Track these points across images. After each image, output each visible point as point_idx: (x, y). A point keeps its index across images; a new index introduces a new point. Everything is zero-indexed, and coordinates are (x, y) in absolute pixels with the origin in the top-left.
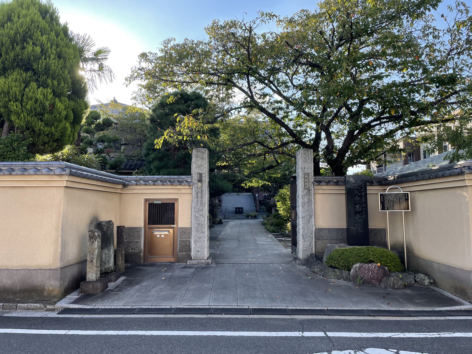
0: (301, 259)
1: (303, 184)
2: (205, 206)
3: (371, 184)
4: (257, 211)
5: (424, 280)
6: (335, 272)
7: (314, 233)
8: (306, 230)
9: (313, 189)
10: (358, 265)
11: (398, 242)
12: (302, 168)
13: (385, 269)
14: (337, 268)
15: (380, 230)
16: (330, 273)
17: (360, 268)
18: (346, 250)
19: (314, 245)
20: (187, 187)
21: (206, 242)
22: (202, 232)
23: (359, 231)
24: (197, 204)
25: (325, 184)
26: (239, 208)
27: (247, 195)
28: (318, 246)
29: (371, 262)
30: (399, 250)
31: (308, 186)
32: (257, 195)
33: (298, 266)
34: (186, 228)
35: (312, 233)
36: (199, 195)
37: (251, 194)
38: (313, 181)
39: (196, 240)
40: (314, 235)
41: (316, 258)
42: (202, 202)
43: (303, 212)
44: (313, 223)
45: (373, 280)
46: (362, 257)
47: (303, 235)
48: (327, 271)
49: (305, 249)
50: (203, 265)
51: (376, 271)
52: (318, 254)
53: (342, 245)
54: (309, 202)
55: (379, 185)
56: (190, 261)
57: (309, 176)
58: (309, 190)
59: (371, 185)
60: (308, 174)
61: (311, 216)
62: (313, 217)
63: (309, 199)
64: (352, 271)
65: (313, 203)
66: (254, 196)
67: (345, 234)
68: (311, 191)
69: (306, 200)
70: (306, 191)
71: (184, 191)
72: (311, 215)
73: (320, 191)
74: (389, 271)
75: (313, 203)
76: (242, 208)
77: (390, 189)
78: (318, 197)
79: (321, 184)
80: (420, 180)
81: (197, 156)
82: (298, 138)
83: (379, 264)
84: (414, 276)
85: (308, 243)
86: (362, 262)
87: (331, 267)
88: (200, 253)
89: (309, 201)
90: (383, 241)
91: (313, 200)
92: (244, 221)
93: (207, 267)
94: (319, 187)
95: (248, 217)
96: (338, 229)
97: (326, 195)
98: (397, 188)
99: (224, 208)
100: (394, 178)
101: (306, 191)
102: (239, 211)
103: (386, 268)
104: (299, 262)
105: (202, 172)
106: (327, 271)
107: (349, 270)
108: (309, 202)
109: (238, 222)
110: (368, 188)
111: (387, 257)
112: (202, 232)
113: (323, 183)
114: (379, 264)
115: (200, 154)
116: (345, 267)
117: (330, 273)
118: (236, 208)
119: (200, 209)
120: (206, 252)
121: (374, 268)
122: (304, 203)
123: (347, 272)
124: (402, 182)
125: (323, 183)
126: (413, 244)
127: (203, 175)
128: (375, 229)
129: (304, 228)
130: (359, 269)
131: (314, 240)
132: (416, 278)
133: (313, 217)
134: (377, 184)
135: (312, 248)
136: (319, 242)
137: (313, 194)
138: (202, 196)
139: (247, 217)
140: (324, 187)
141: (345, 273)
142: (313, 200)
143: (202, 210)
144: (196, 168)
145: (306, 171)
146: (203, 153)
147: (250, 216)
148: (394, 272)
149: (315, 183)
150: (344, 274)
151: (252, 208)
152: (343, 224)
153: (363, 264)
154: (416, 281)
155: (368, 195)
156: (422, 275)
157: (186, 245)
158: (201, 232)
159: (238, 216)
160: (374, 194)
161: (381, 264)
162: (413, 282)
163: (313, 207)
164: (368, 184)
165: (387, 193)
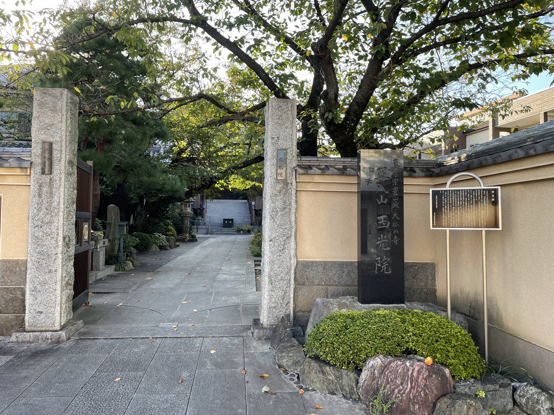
0: (265, 325)
1: (274, 171)
2: (57, 214)
3: (411, 172)
4: (252, 224)
5: (538, 402)
6: (323, 373)
7: (292, 272)
8: (276, 267)
9: (294, 183)
10: (377, 361)
11: (462, 292)
12: (273, 138)
13: (444, 375)
14: (328, 364)
15: (423, 266)
16: (313, 375)
17: (384, 368)
18: (353, 318)
19: (292, 296)
20: (18, 172)
21: (58, 292)
22: (50, 271)
23: (384, 275)
24: (39, 210)
25: (319, 172)
26: (228, 220)
27: (241, 203)
28: (300, 299)
29: (408, 353)
30: (472, 317)
31: (284, 175)
32: (253, 203)
33: (255, 344)
34: (17, 262)
35: (288, 273)
36: (45, 189)
37: (246, 201)
38: (294, 165)
39: (35, 288)
40: (293, 276)
41: (294, 329)
42: (51, 205)
43: (271, 230)
44: (292, 252)
45: (414, 404)
46: (388, 339)
47: (270, 277)
48: (307, 368)
49: (273, 305)
50: (44, 346)
51: (421, 382)
52: (300, 314)
53: (347, 300)
54: (285, 208)
55: (427, 176)
56: (18, 334)
57: (286, 154)
58: (286, 183)
59: (410, 176)
60: (286, 149)
61: (289, 238)
62: (293, 239)
63: (285, 202)
64: (364, 375)
65: (293, 210)
66: (250, 204)
67: (355, 275)
68: (290, 186)
69: (279, 204)
70: (280, 186)
71: (10, 181)
72: (290, 234)
73: (309, 187)
74: (453, 377)
75: (293, 210)
76: (232, 220)
77: (453, 182)
78: (305, 198)
79: (310, 172)
80: (536, 155)
81: (41, 105)
82: (279, 89)
83: (429, 360)
84: (509, 392)
85: (281, 293)
86: (389, 354)
87: (316, 358)
88: (43, 315)
89: (286, 207)
90: (429, 287)
91: (293, 204)
92: (231, 238)
93: (51, 350)
94: (307, 178)
95: (239, 231)
96: (342, 265)
97: (321, 194)
98: (474, 178)
99: (207, 219)
100: (460, 161)
101: (280, 186)
102: (228, 224)
103: (447, 371)
104: (259, 333)
105: (51, 140)
106: (307, 368)
107: (358, 371)
108: (285, 208)
109: (222, 238)
110: (406, 181)
111: (448, 341)
112: (50, 271)
113: (315, 170)
114: (429, 360)
115: (48, 99)
116: (349, 364)
117: (313, 375)
118: (225, 220)
119: (46, 220)
120: (57, 315)
121: (419, 372)
122: (274, 210)
123: (352, 375)
124: (481, 166)
125: (315, 170)
126: (500, 303)
127: (54, 146)
128: (414, 265)
129: (272, 262)
130: (382, 372)
131: (292, 286)
132: (516, 396)
133: (293, 239)
134: (422, 174)
135: (289, 302)
136: (304, 291)
137: (294, 192)
138: (51, 193)
139: (237, 232)
140: (318, 179)
141: (348, 377)
142: (293, 204)
143: (50, 223)
144: (39, 130)
145: (282, 144)
146: (56, 97)
147: (242, 230)
148: (465, 380)
149: (298, 169)
150: (345, 381)
151: (247, 220)
152: (352, 255)
153: (390, 358)
154: (515, 402)
155: (405, 198)
156: (533, 390)
157: (14, 299)
158: (46, 271)
159: (226, 230)
160: (417, 195)
161: (434, 358)
162: (510, 406)
163: (293, 219)
164: (405, 173)
165: (447, 188)
